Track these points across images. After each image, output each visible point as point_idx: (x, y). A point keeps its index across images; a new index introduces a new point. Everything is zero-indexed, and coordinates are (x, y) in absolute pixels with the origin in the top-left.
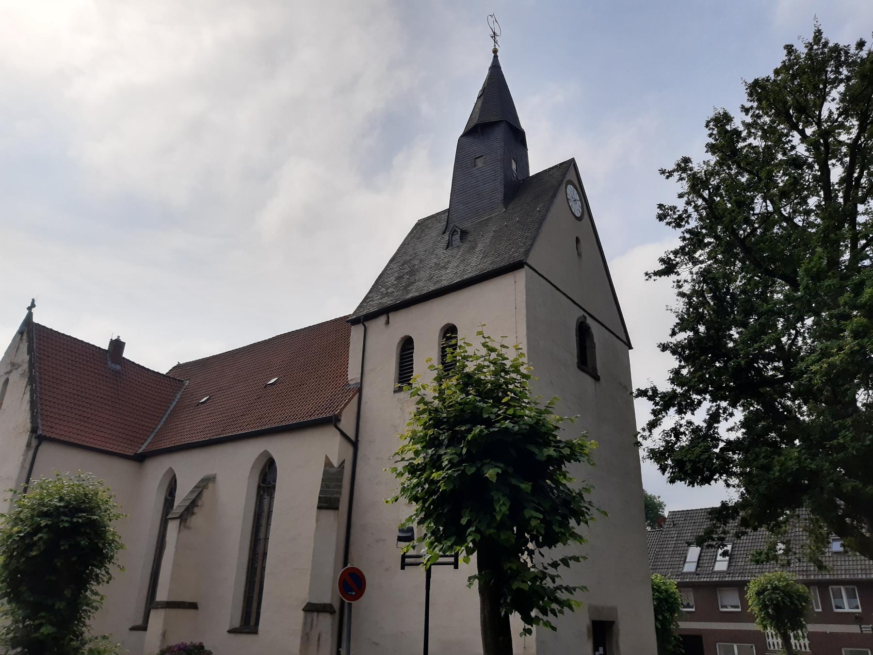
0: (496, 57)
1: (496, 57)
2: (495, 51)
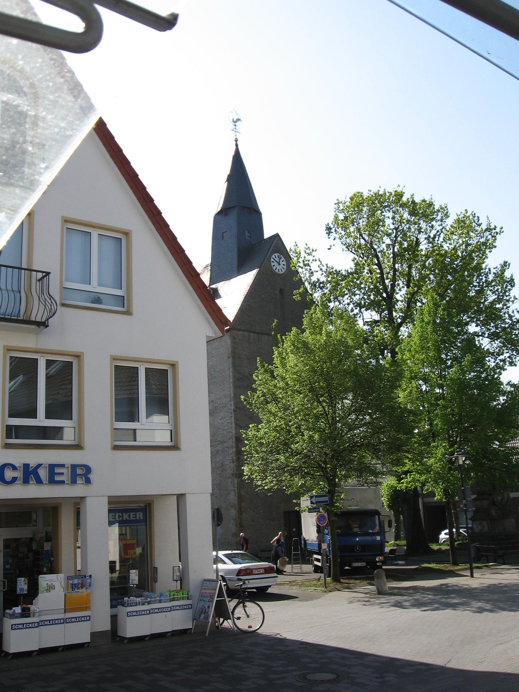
0: (237, 145)
1: (237, 145)
2: (236, 140)
